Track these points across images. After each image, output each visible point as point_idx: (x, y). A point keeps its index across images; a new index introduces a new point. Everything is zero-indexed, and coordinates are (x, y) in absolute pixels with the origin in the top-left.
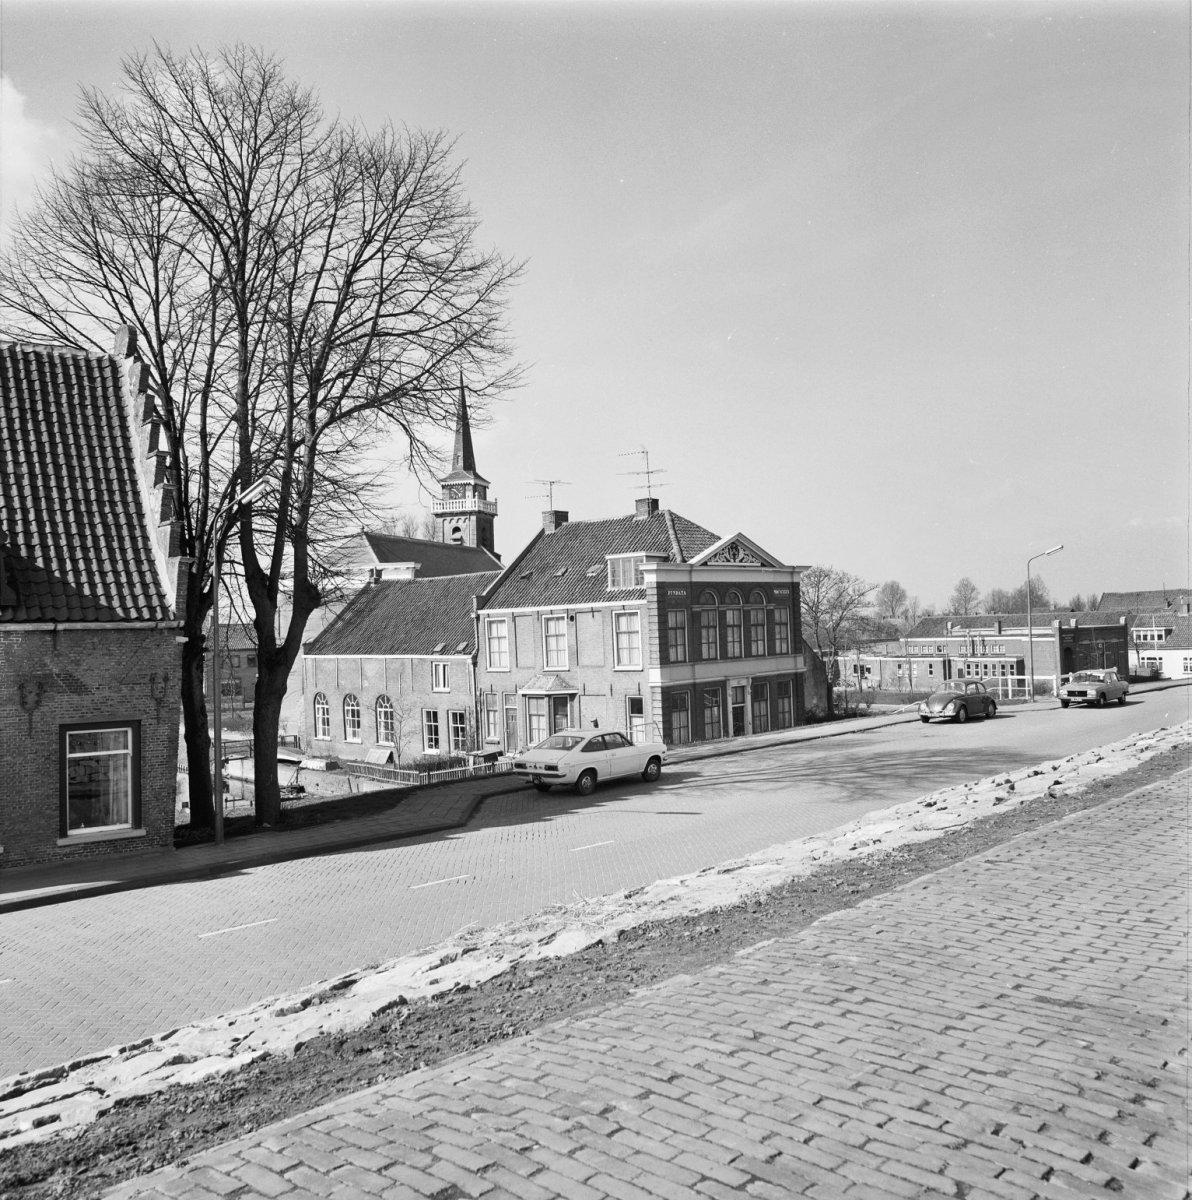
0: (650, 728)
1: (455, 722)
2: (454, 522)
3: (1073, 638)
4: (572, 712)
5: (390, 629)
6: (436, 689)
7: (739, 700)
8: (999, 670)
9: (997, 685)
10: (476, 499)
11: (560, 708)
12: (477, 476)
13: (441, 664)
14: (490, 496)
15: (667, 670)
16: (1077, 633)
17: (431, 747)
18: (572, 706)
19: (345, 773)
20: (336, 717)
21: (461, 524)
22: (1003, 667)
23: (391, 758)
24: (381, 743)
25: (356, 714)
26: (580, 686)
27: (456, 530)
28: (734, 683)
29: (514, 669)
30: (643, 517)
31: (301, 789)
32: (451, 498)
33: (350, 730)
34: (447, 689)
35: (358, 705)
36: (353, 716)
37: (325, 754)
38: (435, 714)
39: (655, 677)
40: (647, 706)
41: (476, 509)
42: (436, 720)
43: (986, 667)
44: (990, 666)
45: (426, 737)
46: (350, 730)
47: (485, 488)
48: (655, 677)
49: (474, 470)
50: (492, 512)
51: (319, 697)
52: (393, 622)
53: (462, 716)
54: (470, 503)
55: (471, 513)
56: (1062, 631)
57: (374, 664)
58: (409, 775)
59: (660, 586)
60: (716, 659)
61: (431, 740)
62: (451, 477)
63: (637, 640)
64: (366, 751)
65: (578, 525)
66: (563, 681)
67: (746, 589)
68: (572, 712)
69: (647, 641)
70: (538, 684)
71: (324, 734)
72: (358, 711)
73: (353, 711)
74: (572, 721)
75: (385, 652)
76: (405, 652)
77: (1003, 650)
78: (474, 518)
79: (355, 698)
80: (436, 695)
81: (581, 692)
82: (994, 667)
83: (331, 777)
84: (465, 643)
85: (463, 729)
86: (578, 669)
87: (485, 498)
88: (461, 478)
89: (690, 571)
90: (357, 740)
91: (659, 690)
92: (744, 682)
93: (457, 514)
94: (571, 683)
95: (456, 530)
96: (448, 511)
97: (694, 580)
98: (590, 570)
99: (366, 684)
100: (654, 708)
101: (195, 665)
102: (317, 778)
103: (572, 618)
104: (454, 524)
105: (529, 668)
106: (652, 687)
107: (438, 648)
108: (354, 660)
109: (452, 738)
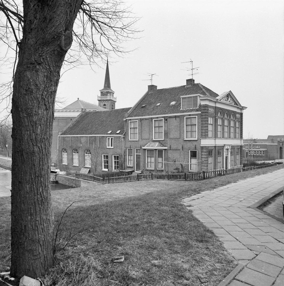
1: (104, 158)
2: (104, 103)
5: (90, 126)
7: (227, 154)
9: (116, 161)
13: (110, 138)
21: (106, 103)
26: (169, 146)
28: (226, 147)
29: (140, 140)
34: (112, 147)
47: (113, 93)
53: (118, 157)
61: (105, 165)
65: (159, 90)
67: (229, 113)
70: (151, 145)
80: (108, 149)
84: (120, 131)
85: (118, 162)
87: (113, 96)
92: (229, 147)
103: (166, 120)
104: (104, 103)
105: (147, 139)
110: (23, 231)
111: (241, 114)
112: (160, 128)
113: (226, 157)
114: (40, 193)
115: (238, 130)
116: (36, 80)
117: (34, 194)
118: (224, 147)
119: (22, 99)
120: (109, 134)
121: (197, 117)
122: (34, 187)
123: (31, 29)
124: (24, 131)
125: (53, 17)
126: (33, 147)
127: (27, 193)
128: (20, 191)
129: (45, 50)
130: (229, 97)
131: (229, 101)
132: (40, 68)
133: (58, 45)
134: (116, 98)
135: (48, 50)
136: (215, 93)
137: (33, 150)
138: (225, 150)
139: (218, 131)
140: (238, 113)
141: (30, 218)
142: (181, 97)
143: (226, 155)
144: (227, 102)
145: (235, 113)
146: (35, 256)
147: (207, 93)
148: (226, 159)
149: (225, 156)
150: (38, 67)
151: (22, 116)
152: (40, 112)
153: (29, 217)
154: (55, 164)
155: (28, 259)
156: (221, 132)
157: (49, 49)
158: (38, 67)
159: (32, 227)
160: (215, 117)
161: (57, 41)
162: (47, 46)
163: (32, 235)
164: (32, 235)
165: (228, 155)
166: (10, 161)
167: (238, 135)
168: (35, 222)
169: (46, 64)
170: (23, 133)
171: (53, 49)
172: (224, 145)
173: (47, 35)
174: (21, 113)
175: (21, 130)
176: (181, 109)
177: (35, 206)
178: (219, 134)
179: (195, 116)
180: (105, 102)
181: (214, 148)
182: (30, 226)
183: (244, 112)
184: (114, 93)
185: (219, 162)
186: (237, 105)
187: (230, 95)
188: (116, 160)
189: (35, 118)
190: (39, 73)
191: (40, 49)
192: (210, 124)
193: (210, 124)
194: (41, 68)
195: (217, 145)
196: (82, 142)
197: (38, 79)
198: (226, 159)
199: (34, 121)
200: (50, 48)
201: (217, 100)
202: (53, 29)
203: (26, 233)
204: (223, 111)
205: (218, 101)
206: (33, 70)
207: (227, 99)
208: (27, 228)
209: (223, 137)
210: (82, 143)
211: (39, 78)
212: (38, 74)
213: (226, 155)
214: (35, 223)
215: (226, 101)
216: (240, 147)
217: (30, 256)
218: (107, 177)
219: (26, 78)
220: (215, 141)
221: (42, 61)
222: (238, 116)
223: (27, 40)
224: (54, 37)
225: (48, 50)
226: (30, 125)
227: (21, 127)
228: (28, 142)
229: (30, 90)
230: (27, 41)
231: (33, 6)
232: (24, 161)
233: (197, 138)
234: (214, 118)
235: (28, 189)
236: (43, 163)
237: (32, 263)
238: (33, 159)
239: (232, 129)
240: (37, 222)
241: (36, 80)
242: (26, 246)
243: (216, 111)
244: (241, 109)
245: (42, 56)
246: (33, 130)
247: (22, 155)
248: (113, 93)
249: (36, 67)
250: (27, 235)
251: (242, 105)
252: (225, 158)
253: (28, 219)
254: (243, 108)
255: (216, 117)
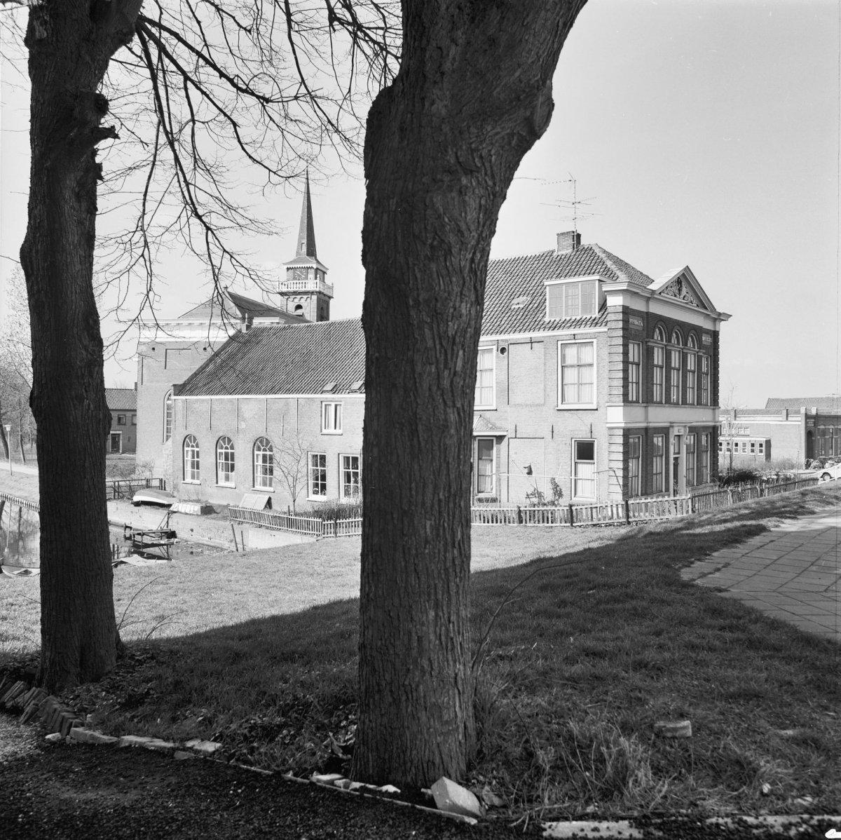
0: (605, 476)
2: (296, 300)
3: (814, 423)
4: (498, 457)
6: (324, 431)
8: (749, 448)
10: (318, 281)
11: (485, 451)
12: (318, 262)
13: (333, 404)
14: (329, 279)
15: (626, 408)
16: (817, 418)
17: (316, 493)
18: (498, 451)
19: (225, 518)
20: (207, 460)
21: (303, 302)
22: (753, 445)
23: (269, 504)
24: (258, 487)
25: (230, 457)
27: (299, 307)
30: (568, 251)
31: (172, 535)
32: (295, 279)
33: (222, 474)
34: (338, 431)
35: (232, 448)
36: (226, 459)
37: (195, 497)
38: (323, 458)
39: (617, 416)
40: (599, 450)
41: (318, 290)
42: (323, 464)
43: (737, 445)
44: (740, 445)
45: (311, 482)
46: (222, 474)
47: (324, 273)
48: (617, 416)
49: (316, 257)
50: (330, 295)
51: (189, 440)
52: (270, 365)
54: (312, 284)
55: (312, 293)
56: (807, 417)
57: (252, 405)
58: (308, 523)
59: (626, 311)
60: (678, 404)
61: (316, 485)
62: (294, 262)
63: (591, 375)
64: (240, 496)
66: (489, 421)
68: (498, 457)
69: (606, 374)
71: (193, 477)
72: (232, 454)
73: (226, 454)
74: (498, 467)
75: (265, 392)
76: (288, 391)
77: (748, 432)
78: (315, 297)
79: (229, 440)
81: (511, 434)
82: (744, 445)
83: (208, 521)
86: (508, 408)
87: (324, 281)
88: (303, 263)
89: (648, 299)
90: (231, 484)
91: (621, 432)
93: (300, 293)
94: (498, 424)
95: (299, 307)
96: (292, 290)
97: (651, 310)
98: (515, 301)
99: (243, 425)
100: (610, 453)
101: (70, 182)
102: (191, 522)
103: (503, 351)
104: (297, 302)
106: (610, 429)
107: (329, 387)
108: (231, 401)
109: (342, 484)
110: (414, 652)
111: (715, 335)
112: (583, 369)
113: (676, 459)
114: (459, 544)
115: (707, 382)
116: (459, 217)
117: (446, 545)
118: (671, 430)
119: (420, 270)
120: (327, 391)
121: (595, 344)
122: (446, 525)
123: (443, 74)
124: (419, 364)
125: (521, 41)
126: (445, 411)
127: (427, 542)
128: (406, 539)
129: (487, 134)
130: (683, 283)
131: (682, 296)
132: (471, 183)
133: (525, 119)
134: (331, 288)
135: (497, 133)
136: (641, 273)
137: (446, 420)
138: (672, 440)
139: (653, 384)
140: (707, 332)
141: (433, 614)
142: (546, 283)
143: (675, 454)
144: (679, 300)
145: (698, 331)
146: (447, 722)
147: (619, 273)
148: (676, 465)
149: (672, 456)
150: (464, 181)
151: (415, 322)
152: (464, 311)
153: (432, 613)
154: (161, 480)
155: (427, 733)
156: (661, 385)
157: (499, 130)
158: (464, 181)
159: (440, 639)
160: (647, 342)
161: (526, 109)
162: (496, 121)
163: (439, 663)
164: (439, 663)
165: (679, 453)
166: (33, 476)
167: (707, 396)
168: (446, 627)
169: (486, 174)
170: (419, 369)
171: (508, 131)
172: (671, 423)
173: (498, 89)
174: (413, 313)
175: (412, 362)
176: (545, 319)
177: (448, 581)
178: (657, 393)
179: (491, 347)
180: (299, 297)
181: (644, 434)
182: (432, 637)
183: (724, 328)
184: (328, 272)
185: (656, 474)
186: (706, 308)
187: (685, 280)
188: (351, 470)
189: (452, 327)
190: (467, 198)
191: (473, 130)
192: (657, 366)
193: (657, 366)
194: (474, 184)
195: (651, 425)
196: (246, 415)
197: (463, 214)
198: (676, 465)
199: (450, 335)
200: (502, 128)
201: (653, 292)
202: (517, 74)
203: (422, 658)
204: (669, 326)
205: (656, 296)
206: (452, 191)
207: (677, 291)
208: (425, 643)
209: (668, 401)
210: (244, 420)
211: (466, 213)
212: (464, 201)
213: (675, 454)
214: (448, 630)
215: (675, 296)
216: (711, 430)
217: (432, 723)
218: (331, 519)
219: (429, 212)
220: (647, 413)
221: (479, 165)
222: (706, 339)
223: (427, 104)
224: (518, 98)
225: (497, 133)
226: (438, 347)
227: (410, 353)
228: (431, 396)
229: (445, 247)
230: (426, 107)
231: (448, 8)
232: (420, 449)
233: (595, 403)
234: (645, 347)
235: (428, 530)
236: (464, 457)
237: (438, 744)
238: (445, 444)
239: (674, 374)
240: (451, 625)
241: (459, 217)
242: (422, 694)
243: (648, 323)
244: (715, 320)
245: (478, 150)
246: (446, 360)
247: (414, 433)
248: (324, 273)
249: (459, 180)
250: (425, 663)
251: (719, 310)
252: (672, 461)
253: (427, 616)
254: (720, 317)
255: (649, 344)
